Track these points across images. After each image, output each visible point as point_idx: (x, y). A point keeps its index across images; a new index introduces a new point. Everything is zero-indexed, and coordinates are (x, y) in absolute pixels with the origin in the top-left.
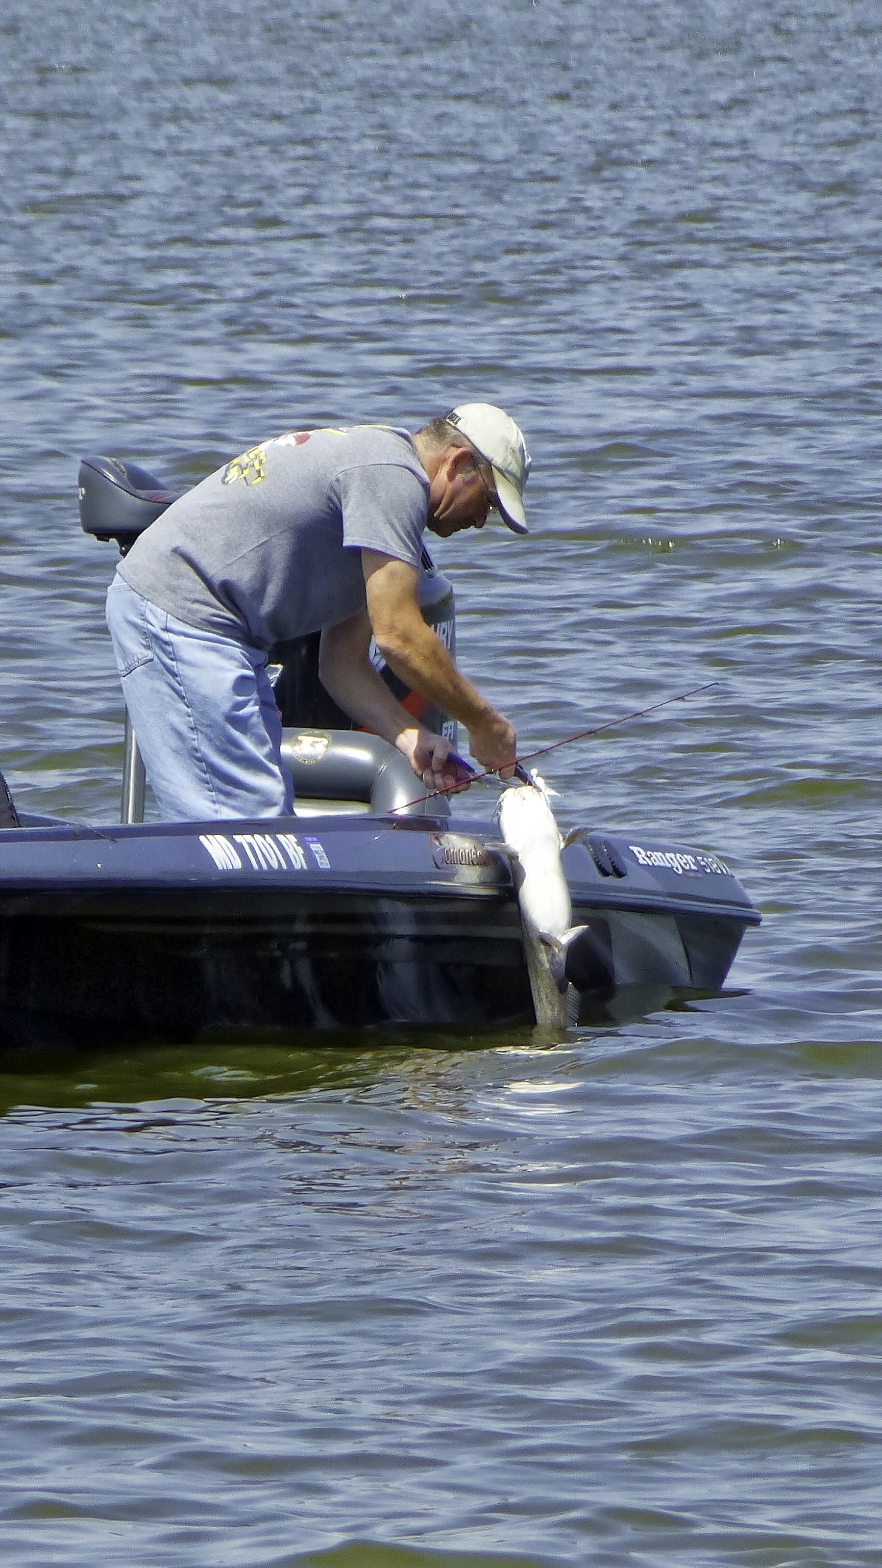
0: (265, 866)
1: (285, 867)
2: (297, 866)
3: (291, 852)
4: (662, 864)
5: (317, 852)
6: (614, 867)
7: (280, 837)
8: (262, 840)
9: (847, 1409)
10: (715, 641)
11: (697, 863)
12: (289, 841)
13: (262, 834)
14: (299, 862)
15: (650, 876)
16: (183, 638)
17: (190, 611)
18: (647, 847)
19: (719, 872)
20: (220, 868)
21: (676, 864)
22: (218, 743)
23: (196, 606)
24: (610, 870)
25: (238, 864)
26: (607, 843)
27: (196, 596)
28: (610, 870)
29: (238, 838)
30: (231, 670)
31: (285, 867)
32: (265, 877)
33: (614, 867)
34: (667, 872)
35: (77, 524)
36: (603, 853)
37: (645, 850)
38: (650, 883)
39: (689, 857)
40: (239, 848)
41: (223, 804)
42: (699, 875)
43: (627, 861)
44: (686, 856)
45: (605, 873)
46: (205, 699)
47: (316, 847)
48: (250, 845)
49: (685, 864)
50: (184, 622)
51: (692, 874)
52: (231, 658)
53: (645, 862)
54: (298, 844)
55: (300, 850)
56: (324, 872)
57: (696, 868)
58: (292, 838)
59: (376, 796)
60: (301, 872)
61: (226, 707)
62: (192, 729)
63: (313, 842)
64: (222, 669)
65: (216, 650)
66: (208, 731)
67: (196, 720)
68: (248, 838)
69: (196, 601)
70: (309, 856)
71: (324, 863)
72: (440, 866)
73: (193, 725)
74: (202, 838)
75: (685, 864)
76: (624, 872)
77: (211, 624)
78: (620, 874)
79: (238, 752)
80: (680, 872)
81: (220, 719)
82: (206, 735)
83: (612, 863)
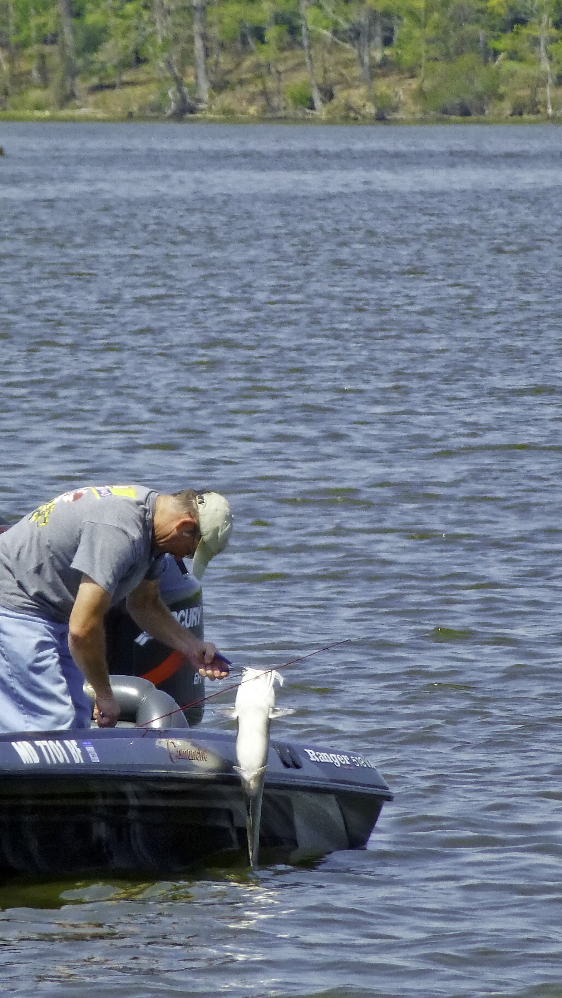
0: (55, 761)
1: (68, 761)
2: (77, 761)
3: (73, 752)
4: (327, 761)
5: (90, 752)
6: (294, 762)
7: (66, 742)
8: (54, 744)
9: (343, 719)
10: (355, 905)
11: (350, 760)
12: (72, 744)
13: (54, 740)
14: (78, 759)
15: (318, 769)
16: (4, 617)
17: (9, 601)
18: (316, 749)
19: (365, 766)
20: (25, 762)
21: (336, 761)
22: (26, 684)
23: (13, 597)
24: (291, 764)
25: (37, 760)
26: (289, 747)
27: (14, 591)
28: (291, 764)
29: (38, 743)
30: (35, 638)
31: (68, 761)
32: (54, 768)
33: (294, 762)
34: (330, 766)
35: (208, 686)
36: (286, 753)
37: (315, 751)
38: (319, 773)
39: (345, 757)
40: (38, 749)
41: (32, 723)
42: (352, 768)
43: (303, 760)
44: (343, 756)
45: (287, 766)
46: (16, 654)
47: (90, 749)
48: (45, 747)
49: (342, 761)
50: (4, 607)
51: (348, 768)
52: (36, 629)
53: (315, 760)
54: (78, 746)
55: (79, 751)
56: (95, 764)
57: (349, 763)
58: (74, 742)
59: (141, 719)
60: (80, 765)
61: (30, 660)
62: (10, 676)
63: (88, 745)
64: (29, 637)
65: (26, 625)
66: (19, 677)
67: (12, 670)
68: (44, 742)
69: (13, 594)
70: (85, 754)
71: (95, 759)
72: (175, 761)
73: (10, 673)
74: (13, 744)
75: (342, 761)
76: (300, 765)
77: (22, 609)
78: (298, 767)
79: (39, 690)
80: (339, 765)
81: (26, 669)
82: (18, 680)
83: (292, 759)
